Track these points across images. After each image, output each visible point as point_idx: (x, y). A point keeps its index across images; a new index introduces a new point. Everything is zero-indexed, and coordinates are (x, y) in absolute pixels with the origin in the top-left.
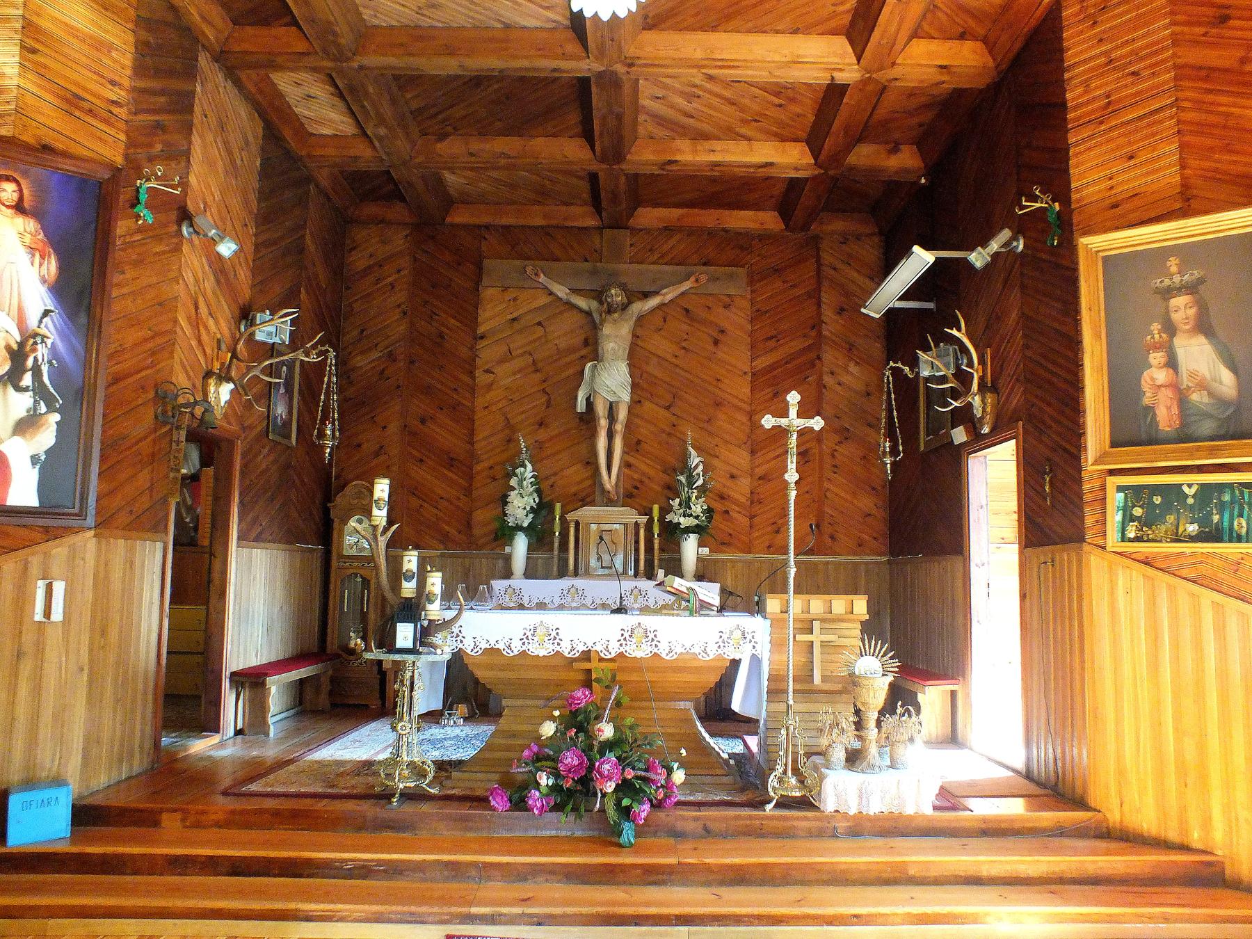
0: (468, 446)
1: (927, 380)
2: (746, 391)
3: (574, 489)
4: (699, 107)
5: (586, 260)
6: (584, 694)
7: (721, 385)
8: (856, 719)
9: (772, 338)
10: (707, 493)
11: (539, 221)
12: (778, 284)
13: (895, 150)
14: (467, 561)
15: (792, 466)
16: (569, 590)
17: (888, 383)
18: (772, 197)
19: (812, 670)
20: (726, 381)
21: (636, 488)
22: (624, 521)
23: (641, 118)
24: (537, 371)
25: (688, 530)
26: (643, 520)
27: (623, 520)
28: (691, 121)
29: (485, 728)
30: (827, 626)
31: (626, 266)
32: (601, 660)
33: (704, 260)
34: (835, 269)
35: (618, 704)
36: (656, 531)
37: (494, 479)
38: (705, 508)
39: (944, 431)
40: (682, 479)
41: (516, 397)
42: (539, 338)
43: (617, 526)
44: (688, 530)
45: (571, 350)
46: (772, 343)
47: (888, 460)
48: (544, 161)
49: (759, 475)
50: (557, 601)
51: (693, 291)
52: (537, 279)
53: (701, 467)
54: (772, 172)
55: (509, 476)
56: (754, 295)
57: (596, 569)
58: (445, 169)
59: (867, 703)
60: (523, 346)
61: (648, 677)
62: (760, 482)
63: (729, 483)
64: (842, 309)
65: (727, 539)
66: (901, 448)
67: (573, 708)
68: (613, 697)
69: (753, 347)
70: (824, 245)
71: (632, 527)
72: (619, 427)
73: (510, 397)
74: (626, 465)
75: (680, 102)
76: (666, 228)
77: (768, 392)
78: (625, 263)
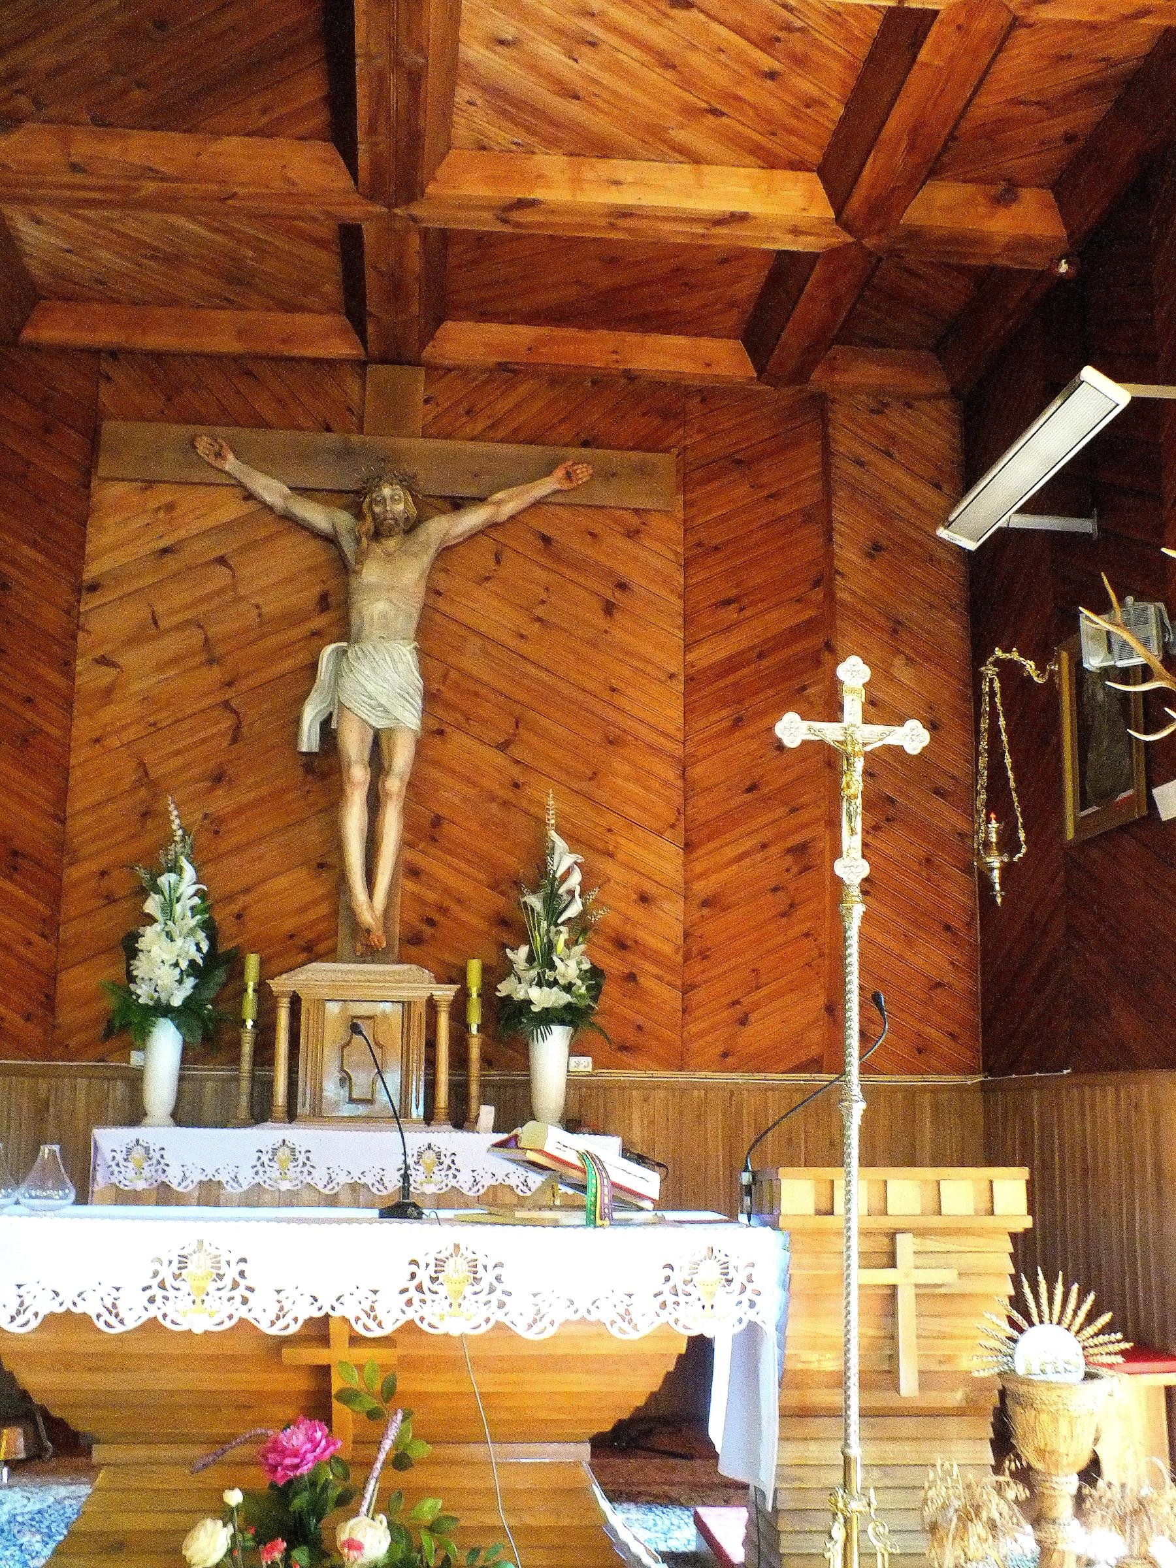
0: (48, 825)
1: (1106, 673)
2: (671, 713)
3: (289, 924)
4: (593, 70)
5: (329, 429)
6: (311, 1439)
7: (623, 702)
8: (1023, 1493)
9: (727, 602)
10: (590, 934)
11: (225, 343)
12: (741, 491)
13: (1006, 198)
14: (43, 1085)
15: (852, 841)
16: (275, 1151)
17: (992, 694)
18: (732, 304)
19: (893, 1358)
20: (630, 692)
21: (430, 922)
22: (404, 995)
23: (464, 94)
24: (211, 661)
25: (548, 1017)
26: (445, 993)
27: (404, 993)
28: (572, 109)
29: (62, 1491)
30: (930, 1244)
31: (417, 443)
32: (356, 1340)
33: (583, 437)
34: (860, 463)
35: (400, 1461)
36: (475, 1019)
37: (110, 899)
38: (586, 966)
39: (1130, 792)
40: (535, 902)
41: (164, 718)
42: (220, 592)
43: (388, 1007)
44: (548, 1017)
45: (291, 618)
46: (730, 614)
47: (995, 861)
48: (240, 191)
49: (703, 896)
50: (247, 1179)
51: (560, 499)
52: (217, 464)
53: (576, 879)
54: (745, 237)
55: (142, 893)
57: (336, 1105)
58: (12, 200)
59: (1052, 1453)
60: (185, 608)
61: (478, 1382)
62: (706, 911)
63: (636, 912)
64: (877, 548)
65: (632, 1037)
66: (1022, 836)
67: (280, 1478)
68: (387, 1445)
69: (688, 620)
70: (839, 415)
71: (420, 1009)
72: (394, 785)
73: (151, 719)
74: (409, 870)
75: (551, 53)
77: (721, 717)
78: (414, 435)
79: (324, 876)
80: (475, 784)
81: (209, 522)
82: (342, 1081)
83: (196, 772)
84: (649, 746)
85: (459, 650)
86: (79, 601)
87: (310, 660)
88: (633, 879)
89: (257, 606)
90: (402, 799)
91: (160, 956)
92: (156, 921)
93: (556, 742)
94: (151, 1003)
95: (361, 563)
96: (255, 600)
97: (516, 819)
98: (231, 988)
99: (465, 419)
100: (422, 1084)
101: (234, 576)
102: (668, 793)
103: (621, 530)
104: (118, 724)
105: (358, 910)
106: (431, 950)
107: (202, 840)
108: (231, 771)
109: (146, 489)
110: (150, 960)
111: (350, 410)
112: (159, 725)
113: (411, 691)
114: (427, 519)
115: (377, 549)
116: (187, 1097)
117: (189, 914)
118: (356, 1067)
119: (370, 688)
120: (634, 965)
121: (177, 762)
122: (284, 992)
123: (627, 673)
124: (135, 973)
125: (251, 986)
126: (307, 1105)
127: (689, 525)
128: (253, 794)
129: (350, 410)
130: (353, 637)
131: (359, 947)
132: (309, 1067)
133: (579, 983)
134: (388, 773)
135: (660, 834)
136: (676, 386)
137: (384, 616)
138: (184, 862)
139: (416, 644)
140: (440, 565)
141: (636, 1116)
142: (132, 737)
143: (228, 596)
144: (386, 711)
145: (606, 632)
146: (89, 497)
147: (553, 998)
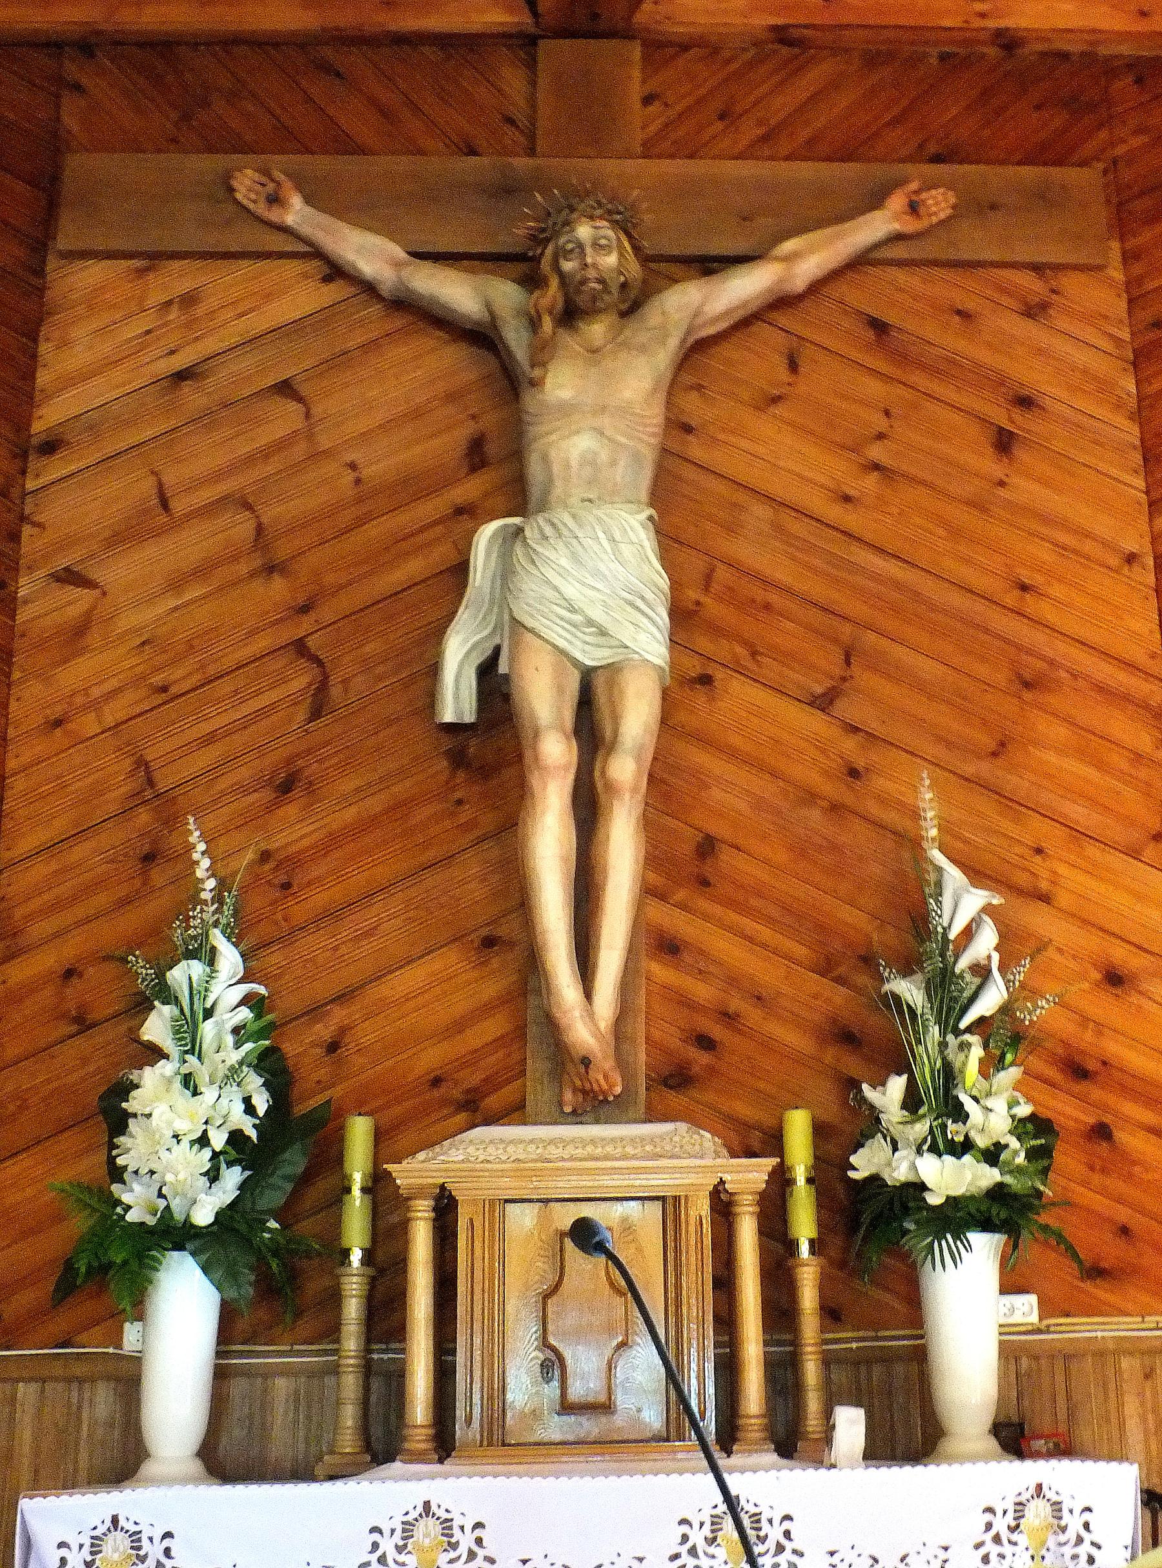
3: (431, 1058)
5: (472, 152)
7: (1045, 610)
20: (1057, 591)
21: (705, 1042)
24: (270, 569)
31: (631, 166)
37: (83, 1023)
41: (181, 675)
51: (899, 252)
52: (274, 215)
53: (986, 943)
55: (142, 1006)
56: (1137, 269)
60: (218, 476)
65: (1111, 1250)
71: (702, 1207)
73: (157, 679)
76: (781, 35)
79: (495, 963)
80: (774, 774)
81: (259, 322)
82: (546, 1368)
83: (243, 774)
84: (1101, 689)
85: (731, 529)
86: (23, 472)
87: (454, 558)
88: (1091, 942)
89: (353, 466)
90: (640, 797)
91: (170, 1123)
92: (166, 1057)
93: (920, 686)
94: (151, 1221)
95: (544, 365)
96: (349, 457)
97: (856, 836)
98: (323, 1186)
99: (720, 126)
100: (710, 1367)
101: (308, 415)
102: (1143, 773)
103: (1014, 305)
104: (96, 692)
105: (564, 1021)
106: (710, 1097)
107: (257, 901)
108: (313, 769)
109: (147, 269)
110: (150, 1133)
111: (510, 121)
112: (174, 690)
113: (649, 596)
114: (659, 291)
115: (567, 339)
116: (238, 1410)
117: (230, 1040)
118: (579, 1334)
119: (571, 590)
120: (1105, 1108)
121: (206, 758)
122: (422, 1188)
123: (1045, 554)
124: (120, 1161)
125: (358, 1180)
126: (476, 1423)
127: (1136, 292)
128: (353, 810)
129: (510, 121)
130: (531, 506)
131: (568, 1096)
132: (477, 1341)
133: (1014, 1143)
134: (612, 747)
135: (1134, 853)
136: (1088, 57)
137: (589, 460)
138: (218, 939)
139: (651, 511)
140: (687, 379)
141: (1131, 1407)
142: (122, 715)
143: (299, 450)
144: (603, 633)
145: (1002, 484)
146: (41, 290)
147: (969, 1176)
